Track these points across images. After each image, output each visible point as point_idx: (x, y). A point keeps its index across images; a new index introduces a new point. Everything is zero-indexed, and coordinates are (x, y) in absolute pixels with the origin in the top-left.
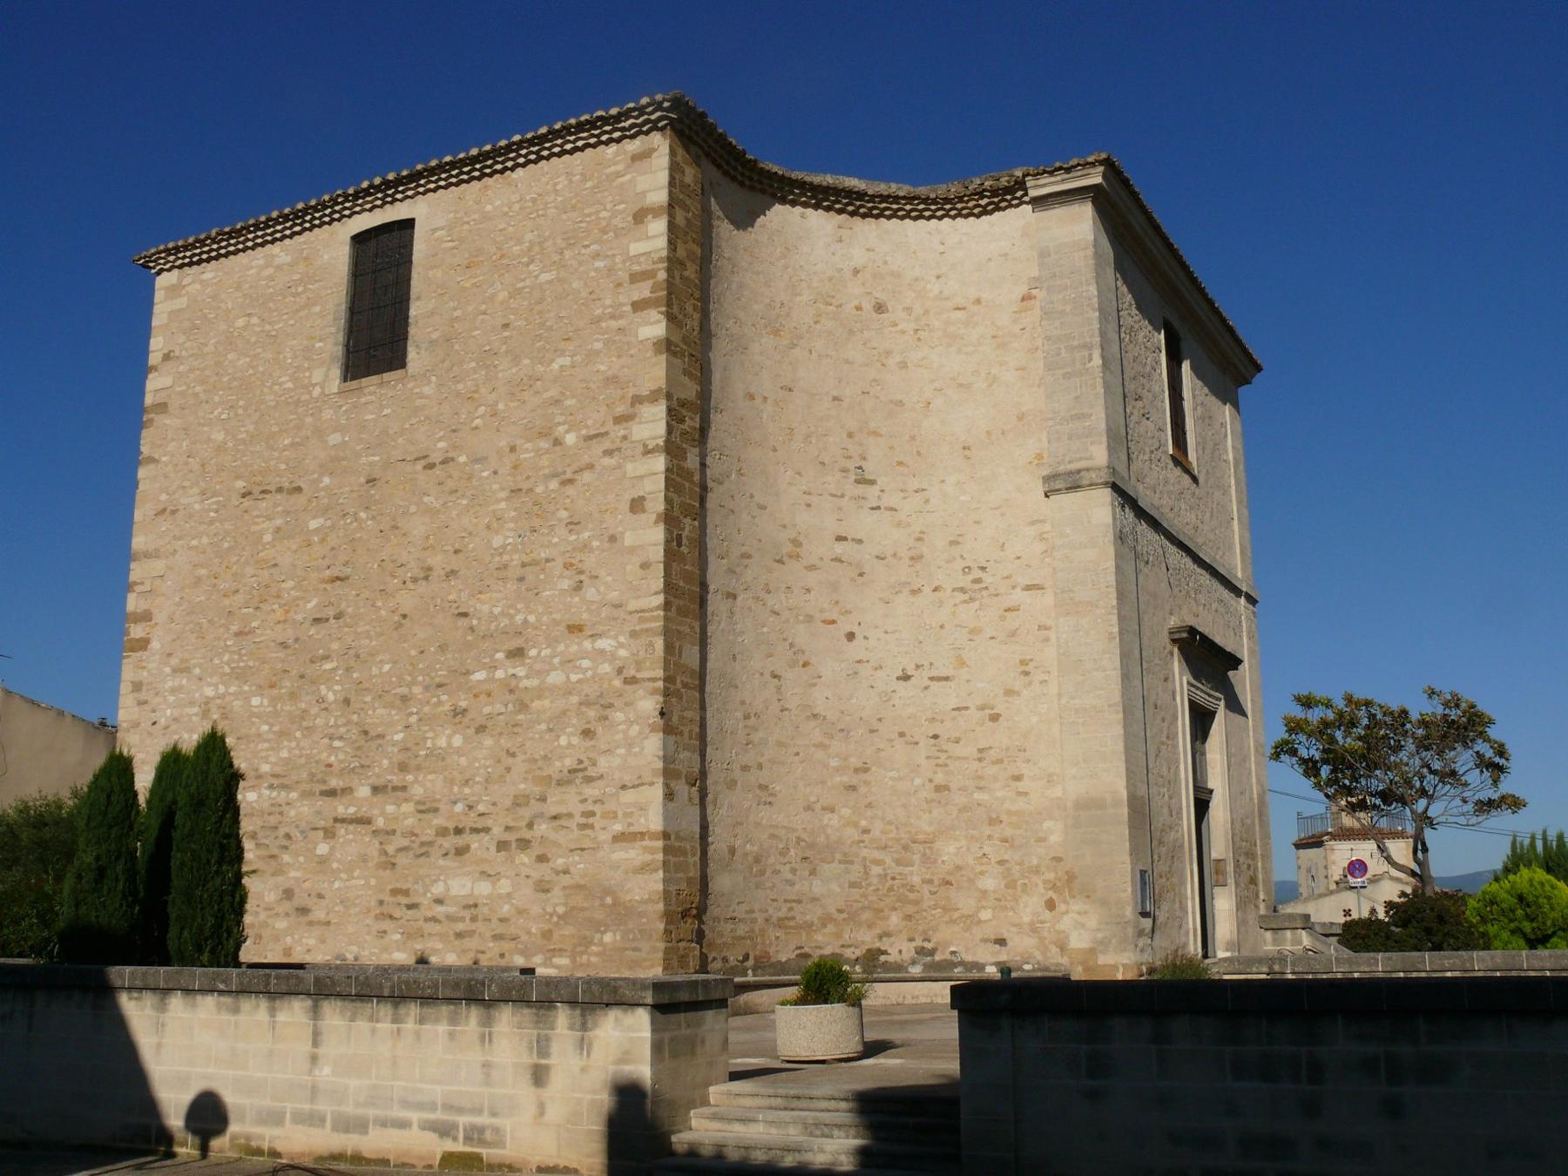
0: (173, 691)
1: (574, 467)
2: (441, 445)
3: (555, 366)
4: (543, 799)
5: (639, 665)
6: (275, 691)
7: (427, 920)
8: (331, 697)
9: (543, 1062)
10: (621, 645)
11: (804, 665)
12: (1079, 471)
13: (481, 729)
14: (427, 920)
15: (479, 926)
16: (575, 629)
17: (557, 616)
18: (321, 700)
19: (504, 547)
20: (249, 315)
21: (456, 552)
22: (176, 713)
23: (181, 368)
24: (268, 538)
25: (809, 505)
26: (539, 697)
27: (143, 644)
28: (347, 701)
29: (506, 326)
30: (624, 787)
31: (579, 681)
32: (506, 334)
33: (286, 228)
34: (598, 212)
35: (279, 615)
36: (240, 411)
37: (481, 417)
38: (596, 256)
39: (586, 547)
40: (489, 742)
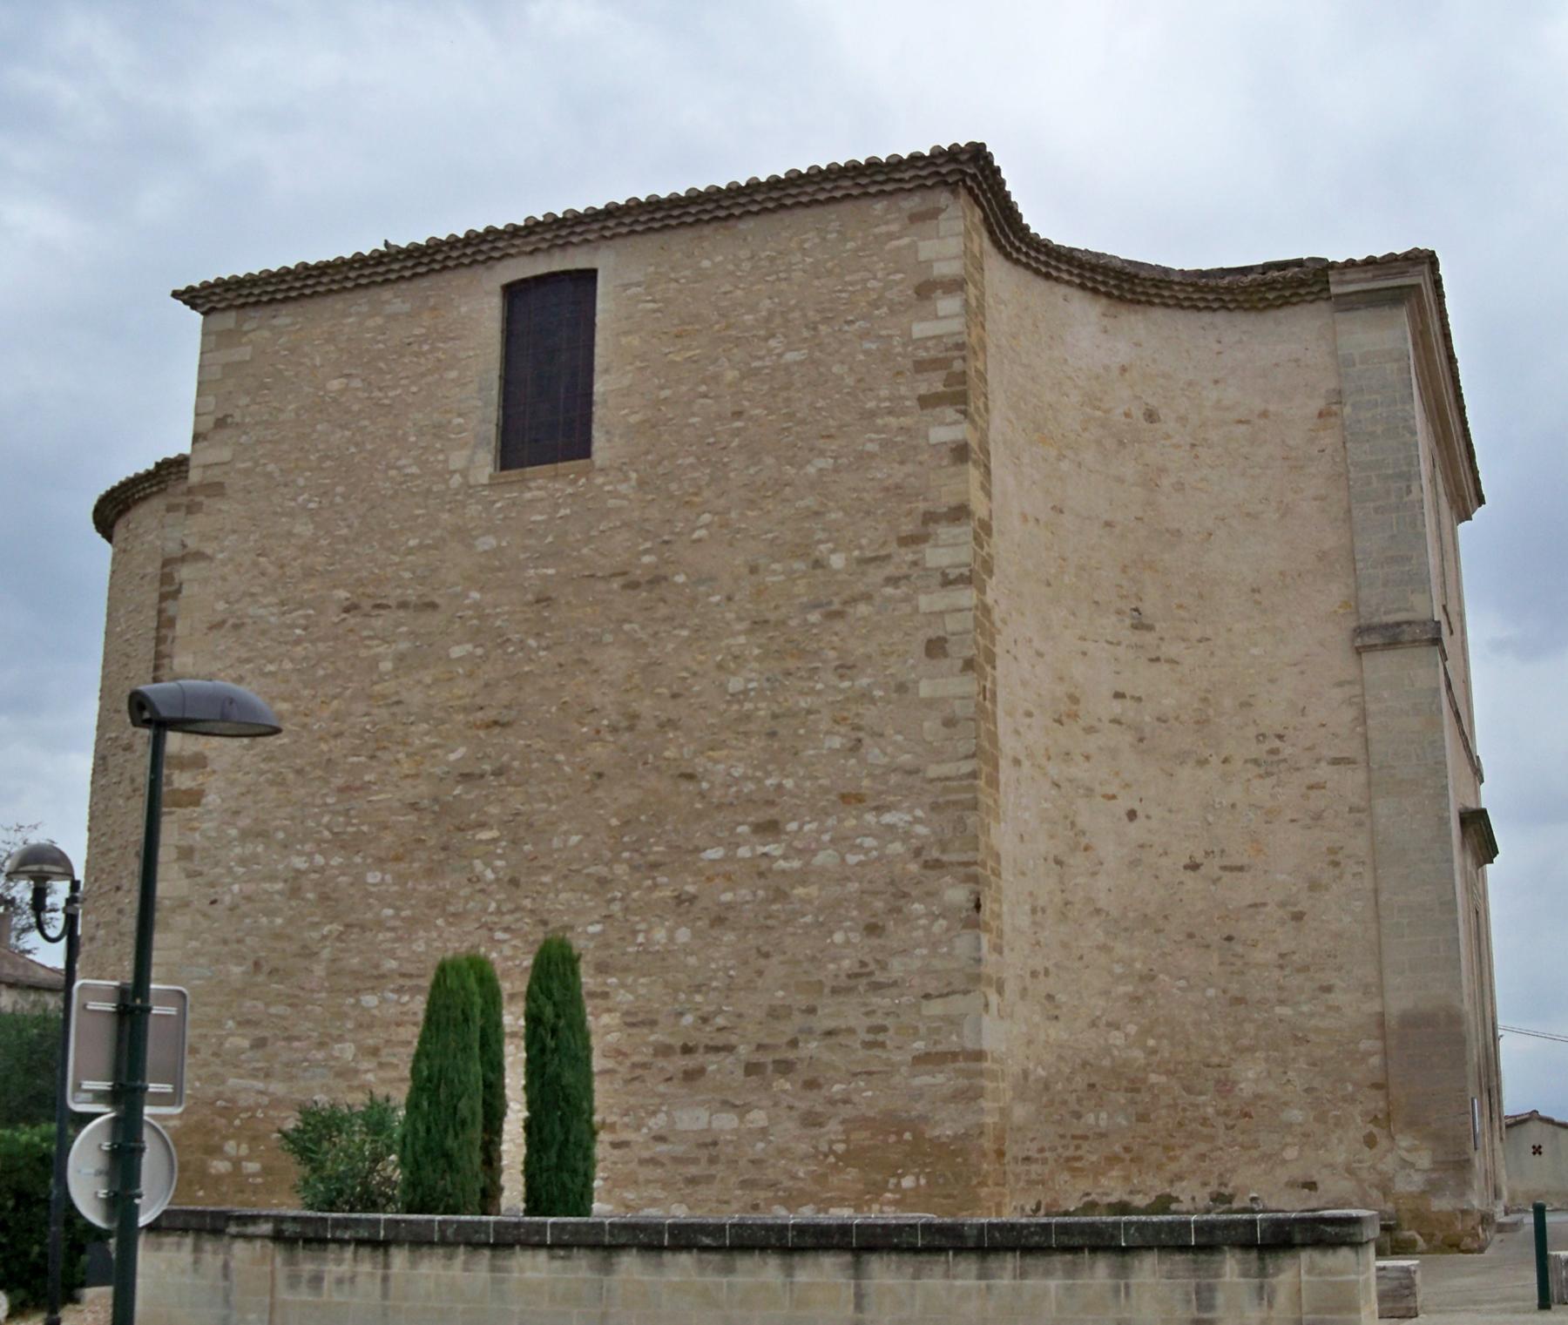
0: (242, 861)
1: (846, 595)
2: (646, 559)
3: (811, 470)
4: (811, 1010)
5: (944, 847)
6: (403, 866)
7: (642, 1162)
8: (490, 875)
9: (1206, 1316)
10: (917, 820)
11: (1086, 849)
12: (1398, 624)
13: (719, 921)
14: (642, 1162)
15: (719, 1170)
16: (852, 799)
17: (825, 782)
18: (475, 880)
19: (745, 692)
20: (348, 376)
21: (675, 696)
22: (250, 888)
23: (244, 439)
24: (386, 666)
25: (1084, 654)
26: (804, 883)
27: (194, 797)
28: (514, 882)
29: (738, 414)
30: (927, 996)
31: (860, 864)
32: (738, 424)
33: (405, 268)
34: (865, 281)
35: (407, 767)
36: (338, 500)
37: (707, 526)
38: (864, 335)
39: (865, 696)
40: (730, 937)
